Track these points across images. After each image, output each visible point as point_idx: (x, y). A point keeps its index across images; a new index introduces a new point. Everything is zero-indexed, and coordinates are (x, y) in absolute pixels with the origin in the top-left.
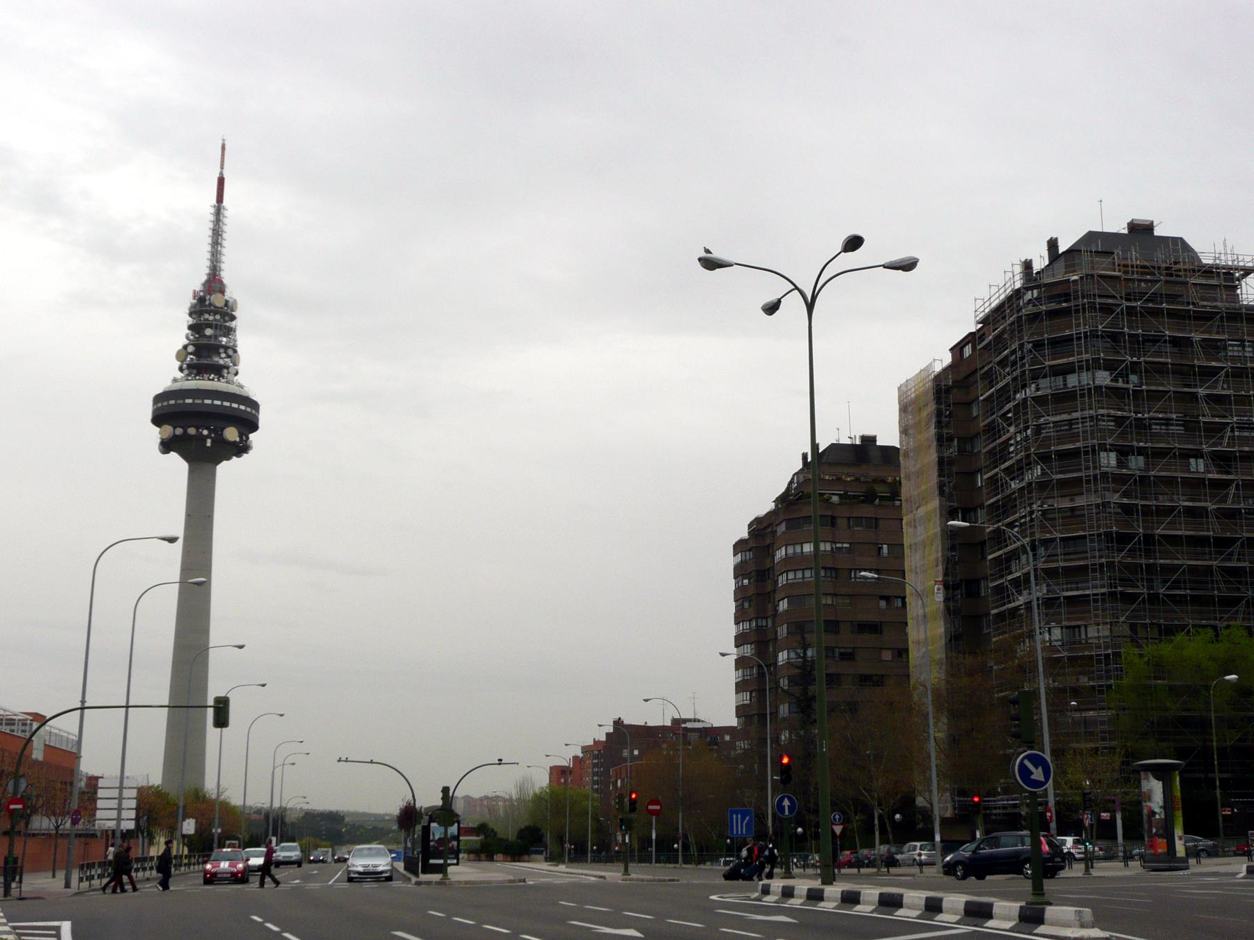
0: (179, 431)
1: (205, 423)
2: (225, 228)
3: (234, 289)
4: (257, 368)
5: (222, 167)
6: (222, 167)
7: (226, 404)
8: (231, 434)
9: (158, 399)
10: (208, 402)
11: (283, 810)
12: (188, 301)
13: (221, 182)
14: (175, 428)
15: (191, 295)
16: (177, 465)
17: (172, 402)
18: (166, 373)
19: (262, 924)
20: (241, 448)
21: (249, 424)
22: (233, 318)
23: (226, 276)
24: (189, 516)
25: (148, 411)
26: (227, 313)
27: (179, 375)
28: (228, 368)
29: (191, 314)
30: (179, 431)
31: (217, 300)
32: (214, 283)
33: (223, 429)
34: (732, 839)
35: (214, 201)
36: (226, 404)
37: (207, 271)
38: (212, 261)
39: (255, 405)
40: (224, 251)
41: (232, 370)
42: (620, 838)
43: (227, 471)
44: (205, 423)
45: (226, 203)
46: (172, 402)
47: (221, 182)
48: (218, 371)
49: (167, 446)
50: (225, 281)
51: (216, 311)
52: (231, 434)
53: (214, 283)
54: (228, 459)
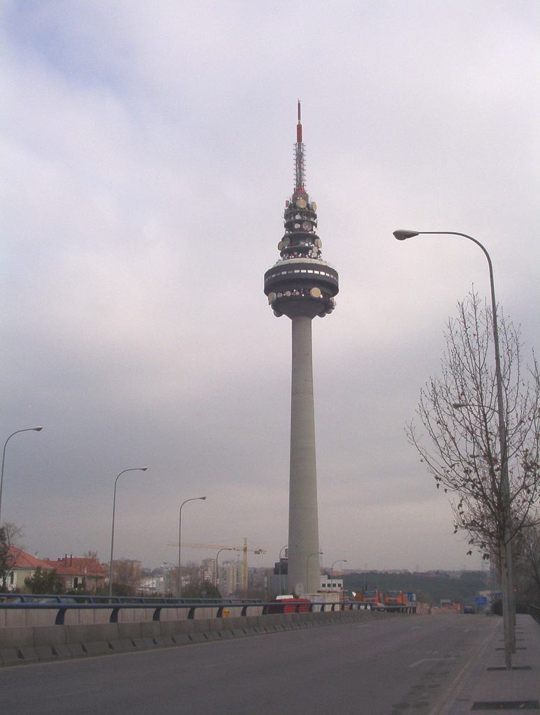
0: (280, 295)
1: (300, 289)
4: (333, 248)
5: (299, 118)
6: (299, 118)
7: (316, 272)
8: (316, 292)
11: (326, 568)
12: (283, 208)
13: (299, 128)
15: (318, 235)
16: (286, 321)
17: (274, 276)
18: (273, 258)
21: (331, 287)
22: (315, 216)
23: (308, 189)
28: (311, 248)
31: (302, 204)
32: (300, 191)
34: (85, 589)
36: (316, 272)
39: (335, 274)
40: (305, 173)
41: (315, 249)
42: (523, 562)
43: (318, 324)
44: (300, 289)
46: (274, 276)
47: (299, 128)
48: (305, 251)
51: (302, 212)
52: (316, 292)
53: (300, 191)
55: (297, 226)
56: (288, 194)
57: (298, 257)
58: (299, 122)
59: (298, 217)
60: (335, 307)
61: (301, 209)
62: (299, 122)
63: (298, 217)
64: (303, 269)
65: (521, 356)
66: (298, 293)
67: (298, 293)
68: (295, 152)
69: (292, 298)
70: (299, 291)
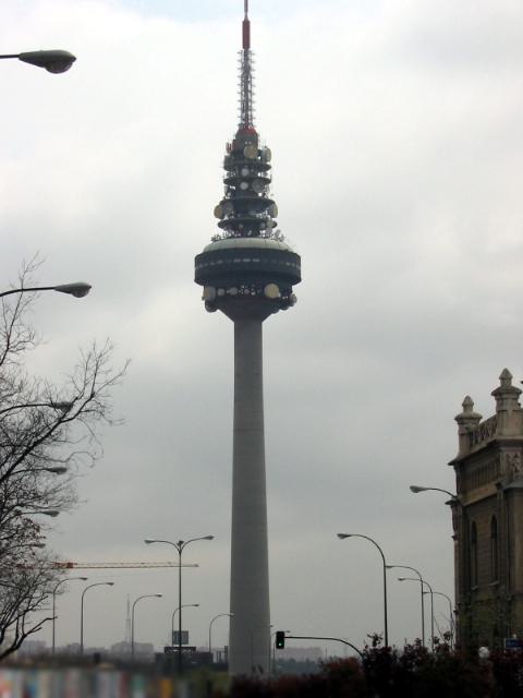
0: (221, 292)
2: (253, 66)
3: (267, 138)
4: (297, 212)
5: (246, 10)
6: (246, 10)
8: (272, 291)
9: (200, 259)
10: (237, 261)
12: (223, 153)
13: (246, 25)
14: (217, 289)
15: (225, 150)
18: (206, 231)
19: (242, 258)
20: (286, 301)
23: (259, 125)
24: (237, 375)
25: (190, 270)
26: (261, 163)
27: (222, 232)
29: (226, 168)
30: (221, 292)
32: (246, 134)
33: (263, 287)
35: (240, 47)
37: (239, 121)
38: (242, 102)
40: (254, 114)
43: (273, 325)
45: (253, 47)
47: (246, 25)
49: (211, 305)
50: (257, 130)
52: (272, 291)
53: (246, 134)
54: (275, 311)
55: (244, 186)
56: (230, 132)
57: (248, 236)
58: (246, 16)
59: (245, 172)
60: (296, 305)
61: (249, 160)
62: (246, 16)
63: (245, 172)
64: (256, 257)
65: (92, 687)
66: (247, 291)
67: (247, 291)
68: (240, 65)
69: (227, 296)
70: (250, 288)
